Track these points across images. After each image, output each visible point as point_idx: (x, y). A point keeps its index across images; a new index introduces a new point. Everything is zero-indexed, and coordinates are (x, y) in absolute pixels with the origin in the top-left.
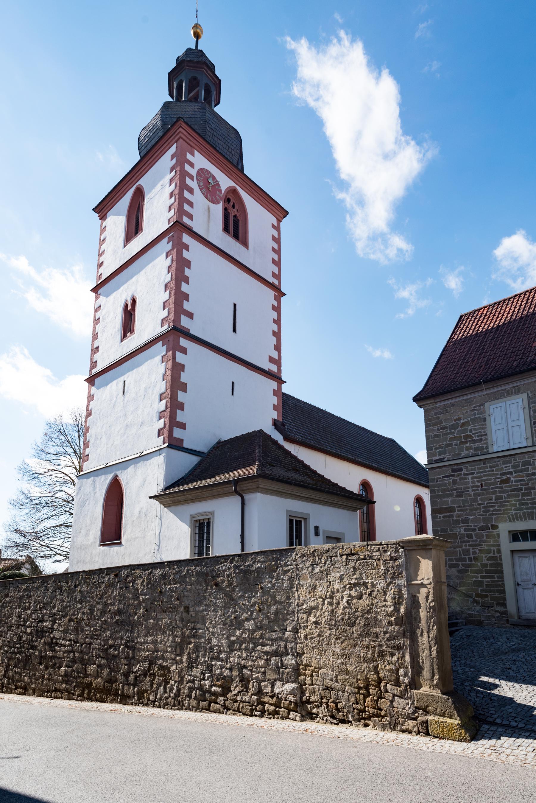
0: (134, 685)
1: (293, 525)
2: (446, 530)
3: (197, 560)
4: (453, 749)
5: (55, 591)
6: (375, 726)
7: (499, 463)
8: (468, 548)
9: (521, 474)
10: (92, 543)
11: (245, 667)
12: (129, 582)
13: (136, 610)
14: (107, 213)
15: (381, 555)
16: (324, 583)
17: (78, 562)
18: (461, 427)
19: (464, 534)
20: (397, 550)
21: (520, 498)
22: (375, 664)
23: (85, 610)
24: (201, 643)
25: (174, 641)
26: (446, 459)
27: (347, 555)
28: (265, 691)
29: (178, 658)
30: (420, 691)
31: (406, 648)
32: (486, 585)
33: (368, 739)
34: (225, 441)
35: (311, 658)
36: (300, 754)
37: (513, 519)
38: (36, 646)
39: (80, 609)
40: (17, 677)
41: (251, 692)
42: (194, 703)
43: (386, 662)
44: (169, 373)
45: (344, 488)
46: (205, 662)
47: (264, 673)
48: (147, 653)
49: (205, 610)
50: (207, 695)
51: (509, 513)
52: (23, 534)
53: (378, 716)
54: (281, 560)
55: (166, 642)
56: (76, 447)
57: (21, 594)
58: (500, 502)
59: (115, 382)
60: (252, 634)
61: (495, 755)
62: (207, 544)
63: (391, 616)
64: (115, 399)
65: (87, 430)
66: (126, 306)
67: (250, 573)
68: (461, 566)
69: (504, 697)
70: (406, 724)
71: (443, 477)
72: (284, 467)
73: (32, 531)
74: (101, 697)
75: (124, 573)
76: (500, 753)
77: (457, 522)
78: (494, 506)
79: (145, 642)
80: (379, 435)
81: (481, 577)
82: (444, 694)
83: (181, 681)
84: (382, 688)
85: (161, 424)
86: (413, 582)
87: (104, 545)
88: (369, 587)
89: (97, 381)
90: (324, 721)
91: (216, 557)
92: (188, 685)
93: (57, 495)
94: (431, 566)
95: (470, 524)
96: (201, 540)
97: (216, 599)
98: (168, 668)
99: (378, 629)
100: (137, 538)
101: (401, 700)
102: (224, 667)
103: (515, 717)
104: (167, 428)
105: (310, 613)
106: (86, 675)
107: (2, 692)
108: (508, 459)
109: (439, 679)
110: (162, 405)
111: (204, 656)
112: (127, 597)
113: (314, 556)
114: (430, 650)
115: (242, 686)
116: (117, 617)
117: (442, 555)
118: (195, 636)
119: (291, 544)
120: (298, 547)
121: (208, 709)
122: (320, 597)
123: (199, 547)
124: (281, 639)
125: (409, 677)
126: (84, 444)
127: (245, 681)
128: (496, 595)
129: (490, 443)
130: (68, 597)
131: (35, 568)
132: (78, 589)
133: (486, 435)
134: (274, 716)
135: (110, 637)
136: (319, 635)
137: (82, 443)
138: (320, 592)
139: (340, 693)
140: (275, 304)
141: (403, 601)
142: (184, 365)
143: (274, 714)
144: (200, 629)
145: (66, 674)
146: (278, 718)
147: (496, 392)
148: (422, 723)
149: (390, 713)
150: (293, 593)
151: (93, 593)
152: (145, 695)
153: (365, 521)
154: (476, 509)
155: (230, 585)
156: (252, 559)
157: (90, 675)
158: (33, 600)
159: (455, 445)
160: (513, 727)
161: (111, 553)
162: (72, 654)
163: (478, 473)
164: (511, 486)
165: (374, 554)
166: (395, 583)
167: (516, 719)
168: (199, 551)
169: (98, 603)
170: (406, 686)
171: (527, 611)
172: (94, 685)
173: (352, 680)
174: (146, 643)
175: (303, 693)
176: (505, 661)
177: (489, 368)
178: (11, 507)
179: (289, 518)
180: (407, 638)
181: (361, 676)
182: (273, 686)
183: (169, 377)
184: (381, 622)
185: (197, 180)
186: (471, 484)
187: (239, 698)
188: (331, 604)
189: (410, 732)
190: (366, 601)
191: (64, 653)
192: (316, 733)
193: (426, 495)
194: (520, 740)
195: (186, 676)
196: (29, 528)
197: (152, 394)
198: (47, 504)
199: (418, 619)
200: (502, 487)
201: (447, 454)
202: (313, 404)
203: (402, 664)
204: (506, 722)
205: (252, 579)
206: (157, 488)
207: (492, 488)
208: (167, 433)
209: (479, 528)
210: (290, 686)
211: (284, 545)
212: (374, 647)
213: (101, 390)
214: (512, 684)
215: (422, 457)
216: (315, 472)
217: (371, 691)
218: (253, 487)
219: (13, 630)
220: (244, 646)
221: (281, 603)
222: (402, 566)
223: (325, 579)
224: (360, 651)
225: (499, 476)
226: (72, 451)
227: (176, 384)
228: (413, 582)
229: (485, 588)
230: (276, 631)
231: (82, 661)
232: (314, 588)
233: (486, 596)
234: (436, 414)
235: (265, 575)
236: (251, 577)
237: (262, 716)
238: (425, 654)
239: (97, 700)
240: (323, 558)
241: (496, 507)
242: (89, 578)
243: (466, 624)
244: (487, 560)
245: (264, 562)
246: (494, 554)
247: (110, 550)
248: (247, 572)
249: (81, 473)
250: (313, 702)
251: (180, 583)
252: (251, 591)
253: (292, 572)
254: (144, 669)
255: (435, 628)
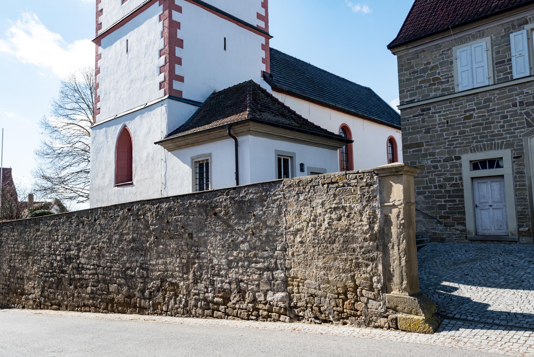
0: (150, 299)
1: (281, 163)
2: (415, 163)
3: (198, 194)
4: (418, 339)
5: (78, 225)
6: (352, 324)
9: (482, 110)
10: (108, 185)
11: (242, 281)
12: (141, 215)
13: (148, 238)
15: (357, 182)
16: (308, 209)
17: (97, 201)
19: (431, 165)
20: (372, 177)
21: (481, 131)
22: (352, 274)
23: (105, 240)
24: (204, 263)
25: (181, 262)
26: (416, 101)
27: (328, 184)
28: (259, 299)
29: (185, 276)
30: (391, 294)
31: (379, 260)
33: (346, 334)
34: (220, 92)
35: (298, 271)
36: (288, 347)
37: (474, 150)
38: (66, 271)
39: (100, 239)
40: (52, 296)
41: (247, 301)
42: (200, 311)
43: (362, 272)
44: (166, 30)
45: (326, 130)
46: (208, 278)
47: (258, 285)
48: (159, 273)
49: (206, 236)
50: (211, 305)
52: (48, 179)
53: (355, 316)
54: (270, 191)
55: (174, 264)
56: (90, 103)
57: (50, 228)
58: (463, 136)
59: (118, 42)
60: (247, 254)
61: (454, 343)
62: (206, 182)
63: (367, 234)
64: (120, 56)
65: (97, 86)
67: (244, 203)
69: (462, 297)
70: (379, 321)
71: (414, 116)
72: (273, 113)
73: (56, 177)
74: (123, 310)
75: (136, 208)
76: (458, 341)
77: (425, 155)
78: (458, 140)
79: (157, 264)
80: (357, 84)
81: (445, 201)
82: (411, 296)
83: (188, 294)
84: (358, 293)
85: (161, 77)
86: (386, 204)
87: (118, 186)
88: (347, 210)
89: (103, 41)
90: (309, 322)
91: (214, 191)
92: (194, 297)
93: (76, 146)
94: (402, 189)
95: (436, 157)
96: (201, 179)
97: (215, 226)
98: (177, 285)
99: (355, 245)
100: (146, 179)
101: (374, 302)
102: (224, 281)
103: (472, 313)
104: (167, 81)
105: (296, 235)
106: (109, 293)
107: (41, 309)
108: (471, 97)
109: (407, 284)
110: (162, 61)
111: (207, 273)
112: (139, 228)
113: (299, 186)
114: (400, 260)
115: (240, 297)
116: (132, 245)
117: (412, 180)
118: (198, 258)
119: (280, 177)
120: (285, 179)
121: (212, 316)
122: (305, 221)
123: (199, 184)
124: (272, 257)
125: (381, 283)
126: (95, 100)
127: (242, 292)
128: (458, 216)
129: (455, 83)
130: (89, 229)
131: (62, 208)
132: (98, 222)
133: (452, 76)
134: (267, 319)
135: (127, 261)
136: (304, 253)
137: (94, 100)
138: (303, 216)
139: (322, 299)
141: (377, 220)
142: (180, 23)
143: (267, 318)
144: (202, 252)
145: (92, 293)
146: (270, 321)
147: (462, 37)
148: (392, 320)
149: (365, 313)
150: (281, 218)
151: (110, 225)
152: (159, 306)
153: (345, 160)
154: (442, 143)
155: (226, 214)
156: (245, 191)
157: (112, 292)
158: (60, 233)
159: (425, 87)
160: (470, 321)
161: (125, 193)
162: (96, 276)
163: (444, 111)
165: (352, 181)
166: (370, 206)
167: (472, 314)
168: (199, 187)
169: (115, 234)
170: (379, 291)
171: (484, 228)
172: (116, 300)
173: (332, 288)
174: (158, 266)
175: (291, 300)
176: (464, 269)
177: (457, 15)
178: (36, 156)
179: (277, 157)
180: (380, 251)
181: (340, 285)
182: (265, 295)
183: (166, 34)
184: (358, 239)
186: (438, 122)
187: (237, 306)
188: (314, 226)
189: (382, 328)
190: (344, 222)
191: (89, 275)
192: (302, 331)
193: (398, 136)
194: (476, 331)
195: (193, 290)
196: (54, 174)
197: (152, 51)
198: (68, 154)
199: (389, 235)
200: (465, 123)
202: (298, 58)
203: (375, 273)
204: (463, 317)
205: (245, 208)
206: (161, 135)
207: (457, 124)
208: (168, 85)
209: (443, 160)
210: (280, 295)
211: (273, 177)
212: (352, 260)
213: (107, 49)
214: (470, 286)
215: (394, 102)
216: (300, 117)
217: (348, 296)
218: (245, 130)
219: (45, 258)
220: (240, 264)
221: (271, 227)
222: (377, 190)
223: (309, 205)
224: (339, 264)
225: (463, 113)
226: (87, 107)
227: (173, 41)
228: (386, 204)
229: (447, 210)
230: (267, 251)
231: (105, 281)
232: (300, 213)
233: (449, 217)
234: (408, 60)
235: (256, 204)
236: (245, 207)
237: (257, 320)
238: (395, 264)
239: (119, 312)
240: (307, 187)
241: (460, 141)
242: (106, 213)
243: (430, 241)
244: (450, 187)
245: (255, 193)
246: (456, 181)
247: (123, 190)
248: (242, 202)
249: (95, 125)
250: (300, 307)
251: (184, 214)
252: (245, 218)
253: (280, 201)
254: (157, 286)
255: (405, 241)
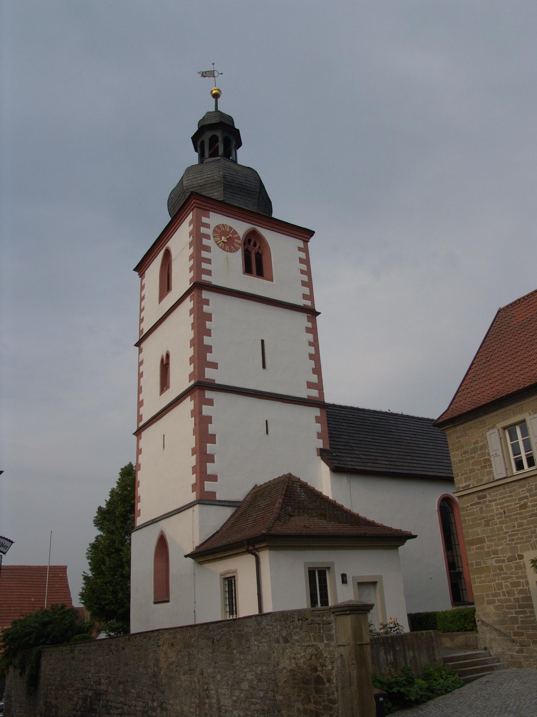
7: (516, 487)
8: (500, 581)
14: (145, 272)
18: (480, 450)
26: (471, 486)
32: (521, 621)
51: (531, 541)
58: (522, 529)
66: (162, 360)
68: (497, 602)
71: (472, 505)
77: (488, 554)
78: (516, 534)
95: (500, 555)
140: (310, 325)
154: (503, 538)
163: (500, 499)
164: (528, 511)
185: (214, 237)
201: (472, 480)
207: (514, 515)
227: (204, 435)
229: (520, 625)
233: (522, 634)
244: (518, 593)
